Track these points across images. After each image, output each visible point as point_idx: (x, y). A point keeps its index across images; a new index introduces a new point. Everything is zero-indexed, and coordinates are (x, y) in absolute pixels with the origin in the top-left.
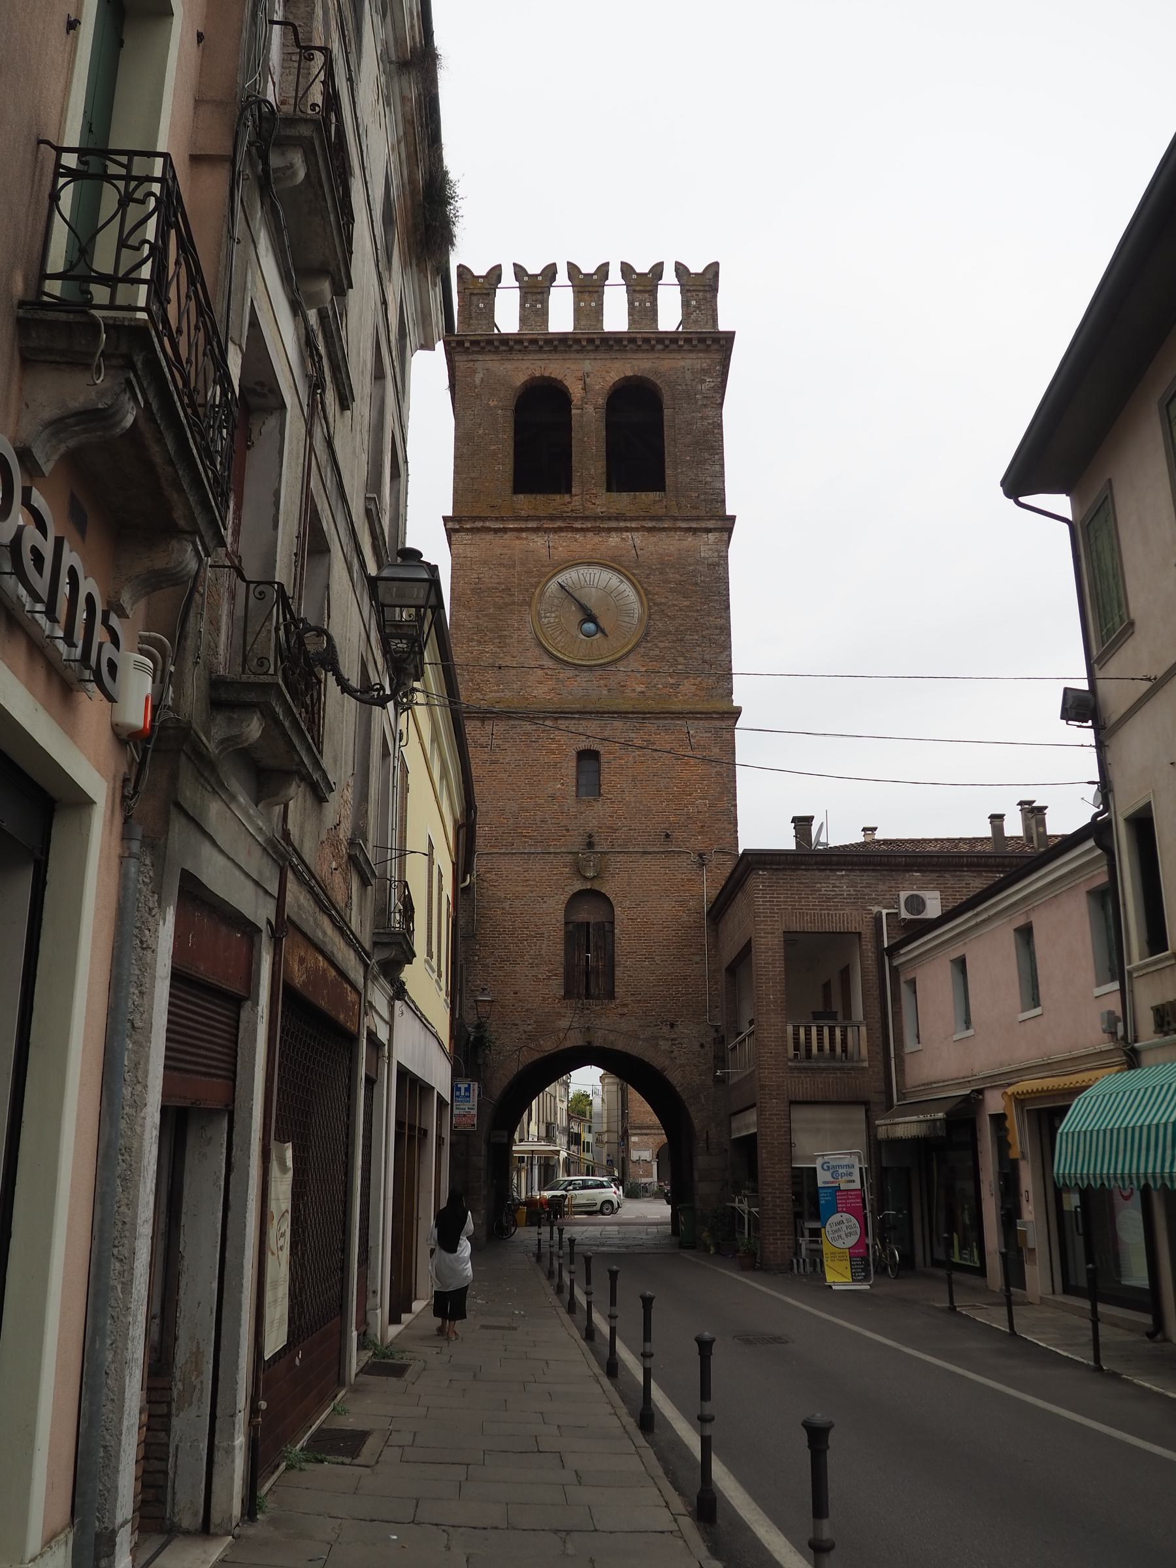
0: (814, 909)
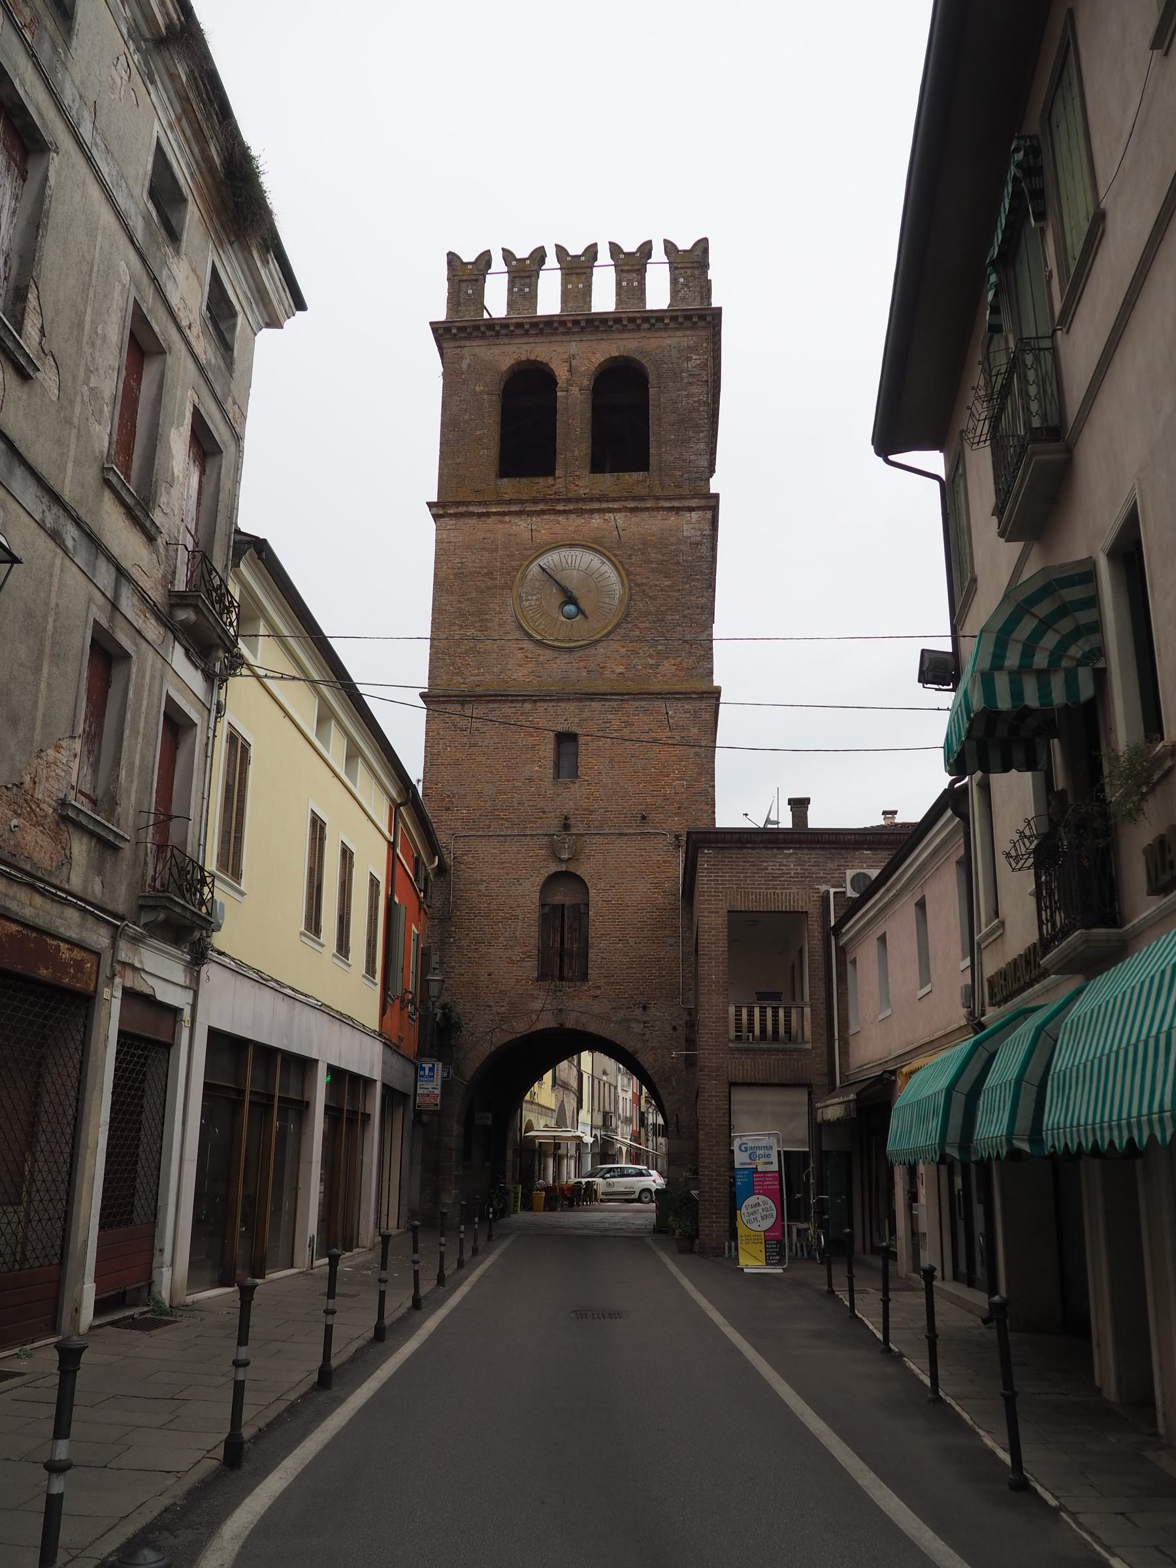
0: (760, 888)
